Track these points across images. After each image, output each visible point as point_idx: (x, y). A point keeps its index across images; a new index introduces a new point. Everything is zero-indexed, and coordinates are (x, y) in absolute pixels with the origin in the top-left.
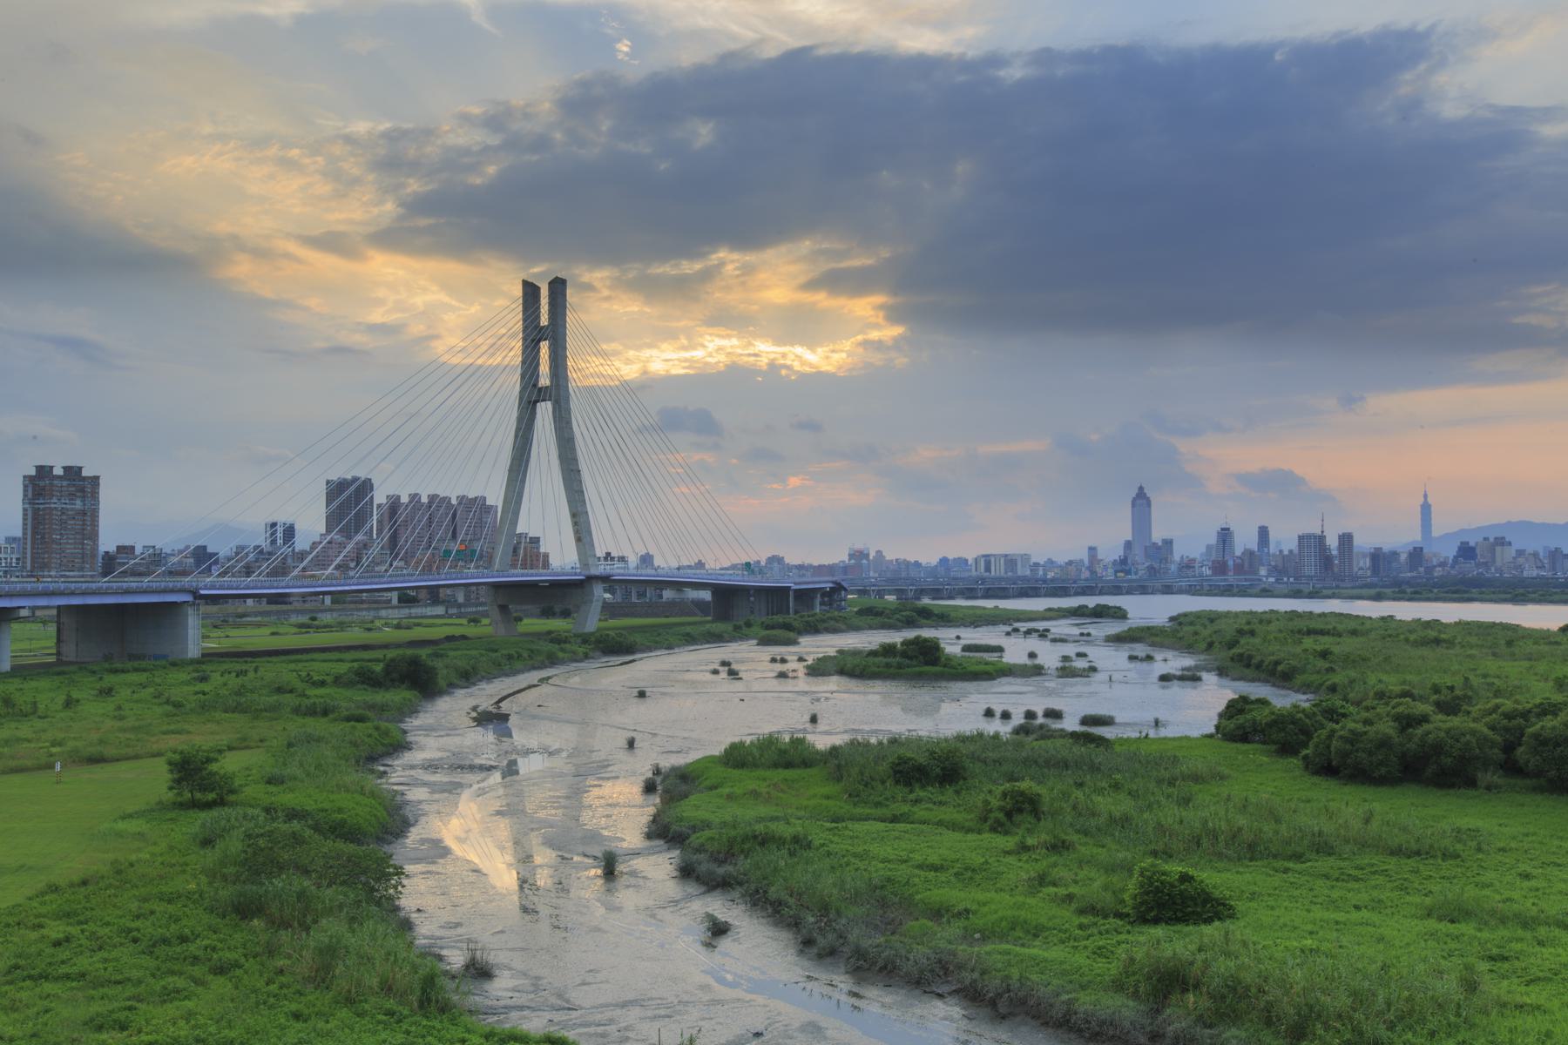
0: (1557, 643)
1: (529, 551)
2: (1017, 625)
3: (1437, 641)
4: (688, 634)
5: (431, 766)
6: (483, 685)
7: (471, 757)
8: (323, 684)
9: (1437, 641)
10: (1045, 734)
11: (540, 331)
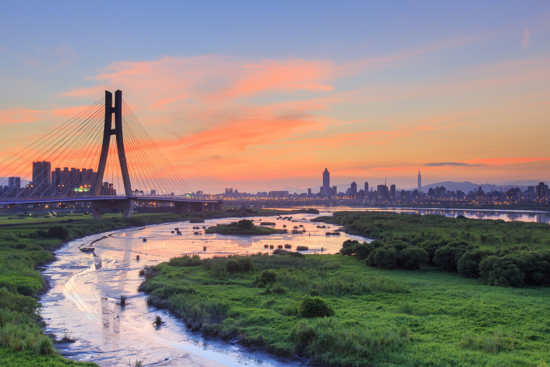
0: (455, 222)
1: (108, 189)
2: (281, 216)
3: (417, 221)
4: (165, 219)
5: (63, 267)
6: (87, 237)
7: (78, 263)
8: (25, 237)
9: (417, 221)
10: (285, 253)
11: (112, 109)
